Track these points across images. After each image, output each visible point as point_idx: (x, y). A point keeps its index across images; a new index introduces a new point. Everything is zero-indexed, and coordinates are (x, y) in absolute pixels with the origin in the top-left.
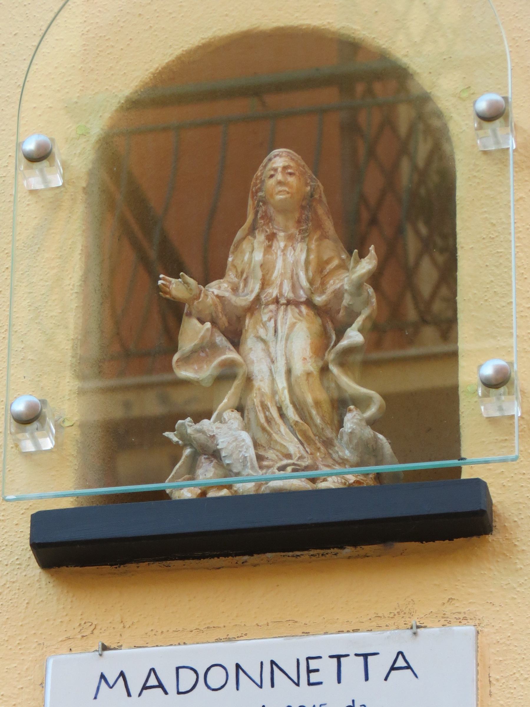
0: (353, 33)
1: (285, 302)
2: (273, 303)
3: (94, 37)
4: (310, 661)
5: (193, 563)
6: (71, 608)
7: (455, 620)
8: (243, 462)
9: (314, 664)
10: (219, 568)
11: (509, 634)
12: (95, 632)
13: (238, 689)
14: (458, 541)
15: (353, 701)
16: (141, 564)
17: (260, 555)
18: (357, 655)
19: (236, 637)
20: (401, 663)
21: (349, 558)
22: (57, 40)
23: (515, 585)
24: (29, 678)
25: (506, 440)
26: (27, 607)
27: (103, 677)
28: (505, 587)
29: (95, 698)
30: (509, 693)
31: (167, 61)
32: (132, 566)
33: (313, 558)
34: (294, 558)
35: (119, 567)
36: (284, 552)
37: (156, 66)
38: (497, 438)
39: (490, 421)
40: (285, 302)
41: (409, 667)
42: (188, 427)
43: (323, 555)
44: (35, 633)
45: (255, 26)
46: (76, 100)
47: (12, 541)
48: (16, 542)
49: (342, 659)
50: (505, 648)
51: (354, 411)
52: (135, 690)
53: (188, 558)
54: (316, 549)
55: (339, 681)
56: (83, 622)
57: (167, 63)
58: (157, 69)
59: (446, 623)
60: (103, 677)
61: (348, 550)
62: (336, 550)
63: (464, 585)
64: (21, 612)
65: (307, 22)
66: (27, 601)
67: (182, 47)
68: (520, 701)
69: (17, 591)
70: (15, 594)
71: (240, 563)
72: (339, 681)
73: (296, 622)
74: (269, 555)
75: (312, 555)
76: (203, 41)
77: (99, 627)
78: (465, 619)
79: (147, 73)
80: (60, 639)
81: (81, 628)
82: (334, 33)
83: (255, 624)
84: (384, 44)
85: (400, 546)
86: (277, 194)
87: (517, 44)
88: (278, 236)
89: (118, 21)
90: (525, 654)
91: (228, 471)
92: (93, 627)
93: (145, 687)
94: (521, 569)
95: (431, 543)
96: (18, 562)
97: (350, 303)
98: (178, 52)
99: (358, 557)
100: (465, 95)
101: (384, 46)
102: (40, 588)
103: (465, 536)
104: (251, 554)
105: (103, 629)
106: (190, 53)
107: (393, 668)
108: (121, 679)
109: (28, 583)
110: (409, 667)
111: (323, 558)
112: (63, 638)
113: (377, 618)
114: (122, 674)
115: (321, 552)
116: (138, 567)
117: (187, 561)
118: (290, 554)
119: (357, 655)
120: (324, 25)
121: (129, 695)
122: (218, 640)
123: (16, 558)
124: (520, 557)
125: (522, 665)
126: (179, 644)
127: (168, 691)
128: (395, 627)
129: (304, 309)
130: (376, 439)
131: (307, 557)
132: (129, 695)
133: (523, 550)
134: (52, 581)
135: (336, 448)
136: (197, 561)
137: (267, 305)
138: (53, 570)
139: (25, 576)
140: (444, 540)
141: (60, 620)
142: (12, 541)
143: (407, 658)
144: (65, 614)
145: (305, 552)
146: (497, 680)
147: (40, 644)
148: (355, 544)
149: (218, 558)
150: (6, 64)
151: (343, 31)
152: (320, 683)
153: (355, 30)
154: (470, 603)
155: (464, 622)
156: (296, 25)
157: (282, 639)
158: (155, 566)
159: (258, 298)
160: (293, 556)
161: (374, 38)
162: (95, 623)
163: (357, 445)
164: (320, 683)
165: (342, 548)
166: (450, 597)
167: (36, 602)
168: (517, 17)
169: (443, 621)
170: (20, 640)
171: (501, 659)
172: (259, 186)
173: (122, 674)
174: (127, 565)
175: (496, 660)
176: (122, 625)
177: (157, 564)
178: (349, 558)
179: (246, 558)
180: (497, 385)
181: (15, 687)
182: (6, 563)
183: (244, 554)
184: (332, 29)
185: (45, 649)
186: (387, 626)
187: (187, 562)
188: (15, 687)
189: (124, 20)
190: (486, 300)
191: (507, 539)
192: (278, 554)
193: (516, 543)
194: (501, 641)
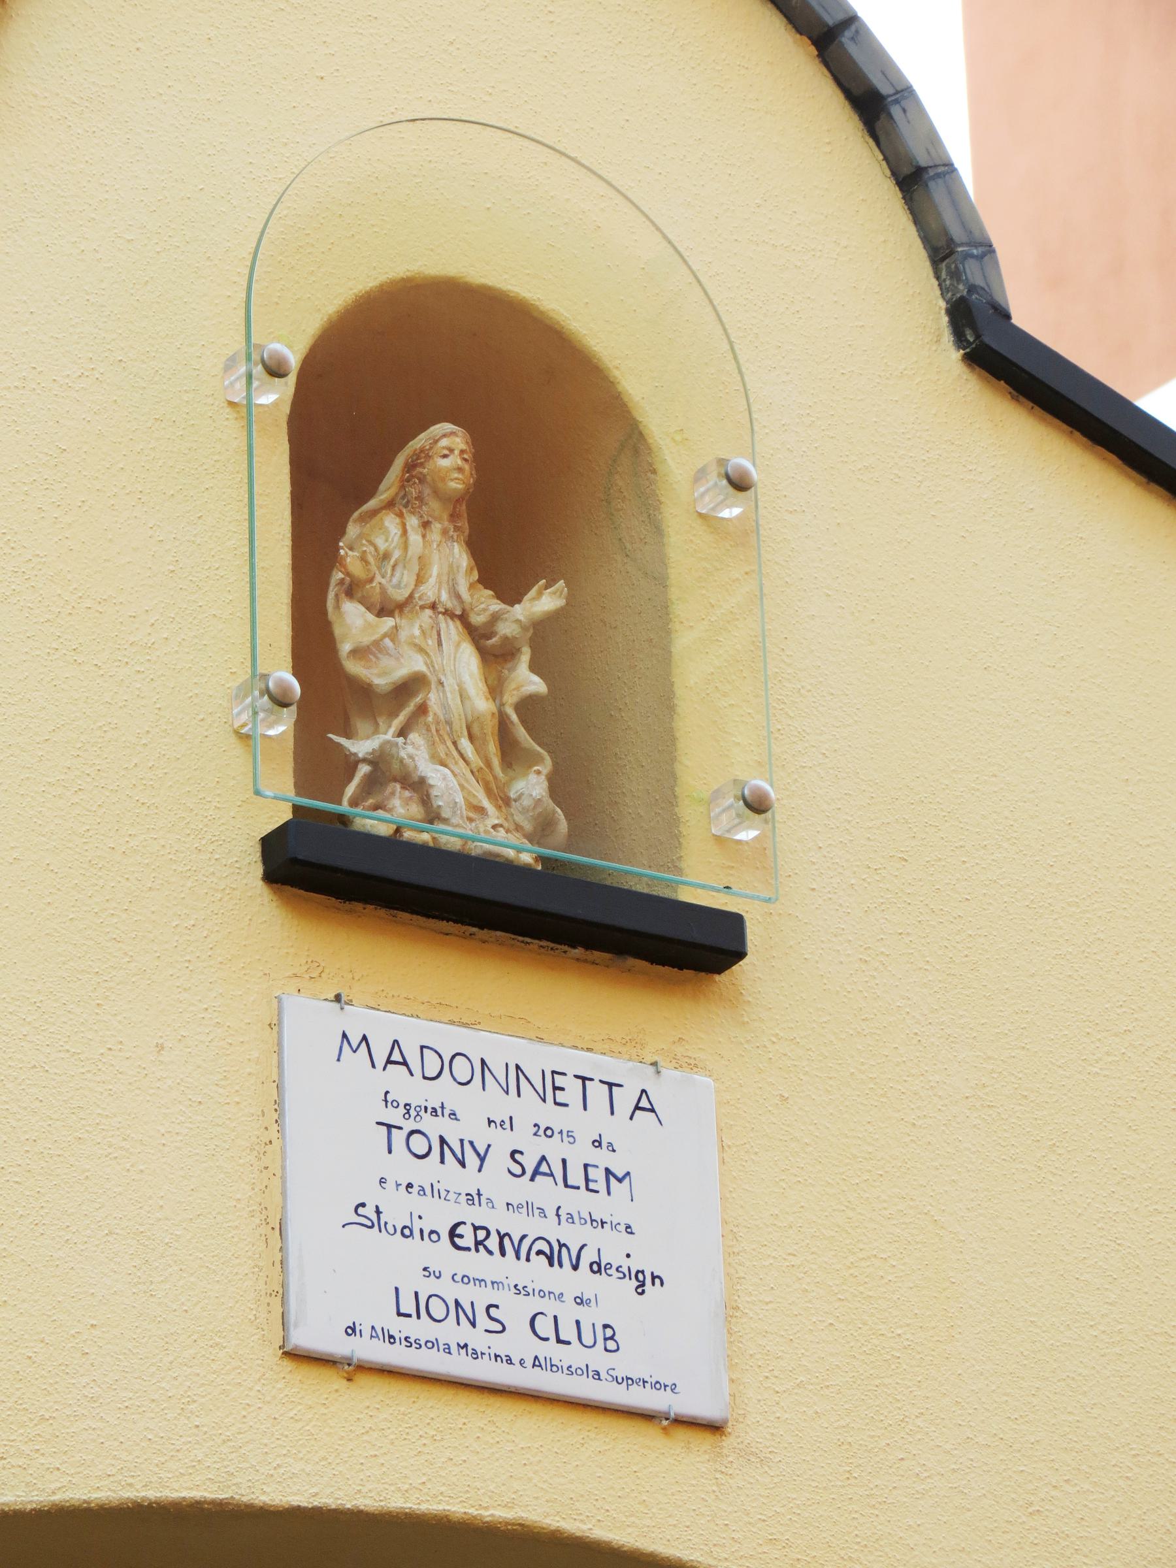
0: (563, 321)
1: (444, 611)
2: (429, 608)
3: (292, 226)
4: (424, 1050)
5: (421, 920)
6: (296, 939)
7: (686, 1065)
8: (453, 808)
9: (559, 1081)
10: (447, 934)
11: (739, 1097)
12: (323, 975)
13: (484, 1089)
14: (688, 973)
15: (600, 1135)
16: (368, 906)
17: (490, 931)
18: (601, 1081)
19: (469, 1023)
20: (644, 1103)
21: (578, 960)
22: (249, 217)
23: (743, 1041)
24: (256, 1013)
25: (733, 867)
26: (249, 924)
27: (344, 1036)
28: (733, 1039)
29: (338, 1060)
30: (741, 1165)
31: (371, 285)
32: (359, 906)
33: (542, 950)
34: (523, 944)
35: (345, 902)
36: (515, 934)
37: (361, 287)
38: (724, 862)
39: (716, 839)
40: (444, 611)
41: (652, 1110)
42: (401, 749)
43: (552, 949)
44: (259, 960)
45: (462, 275)
46: (276, 300)
47: (230, 837)
48: (233, 839)
49: (614, 1088)
50: (735, 1111)
51: (393, 737)
52: (379, 1063)
53: (418, 913)
54: (548, 941)
55: (585, 1109)
56: (310, 960)
57: (371, 288)
58: (361, 291)
59: (677, 1066)
60: (344, 1036)
61: (578, 952)
62: (566, 948)
63: (693, 1026)
64: (243, 929)
65: (516, 289)
66: (249, 917)
67: (386, 273)
68: (751, 1177)
69: (238, 902)
70: (236, 904)
71: (467, 934)
72: (585, 1109)
73: (529, 1022)
74: (499, 933)
75: (541, 946)
76: (409, 274)
77: (327, 971)
78: (696, 1066)
79: (351, 292)
80: (287, 975)
81: (308, 966)
82: (542, 312)
83: (487, 1013)
84: (595, 346)
85: (632, 962)
86: (452, 480)
87: (727, 391)
88: (432, 526)
89: (318, 215)
90: (754, 1124)
91: (433, 816)
92: (320, 969)
93: (389, 1061)
94: (748, 1022)
95: (660, 967)
96: (237, 865)
97: (517, 636)
98: (383, 278)
99: (586, 961)
100: (678, 438)
101: (595, 349)
102: (262, 904)
103: (695, 970)
104: (482, 928)
105: (332, 974)
106: (393, 283)
107: (637, 1108)
108: (364, 1043)
109: (249, 894)
110: (652, 1110)
111: (552, 952)
112: (289, 973)
113: (609, 1041)
114: (364, 1038)
115: (552, 945)
116: (364, 909)
117: (415, 916)
118: (521, 938)
119: (601, 1081)
120: (534, 300)
121: (373, 1066)
122: (452, 1023)
123: (235, 859)
124: (746, 1009)
125: (752, 1135)
126: (412, 1016)
127: (414, 1073)
128: (628, 1057)
129: (458, 623)
130: (554, 812)
131: (536, 946)
132: (373, 1066)
133: (749, 1002)
134: (275, 899)
135: (512, 810)
136: (424, 919)
137: (422, 608)
138: (275, 886)
139: (246, 885)
140: (673, 968)
141: (285, 951)
142: (230, 837)
143: (526, 1073)
144: (291, 944)
145: (537, 941)
146: (729, 1147)
147: (265, 974)
148: (589, 946)
149: (448, 922)
150: (193, 224)
151: (552, 314)
152: (566, 1105)
153: (566, 317)
154: (700, 1049)
155: (695, 1070)
156: (505, 288)
157: (526, 1041)
158: (382, 912)
159: (411, 596)
160: (523, 942)
161: (585, 335)
162: (323, 964)
163: (540, 814)
164: (566, 1105)
165: (574, 947)
166: (680, 1036)
167: (260, 921)
168: (725, 357)
169: (674, 1064)
170: (244, 963)
171: (732, 1123)
172: (422, 460)
173: (364, 1038)
174: (353, 902)
175: (727, 1123)
176: (350, 976)
177: (383, 910)
178: (578, 960)
179: (474, 930)
180: (757, 810)
181: (242, 1020)
182: (224, 863)
183: (474, 926)
184: (542, 308)
185: (271, 982)
186: (620, 1053)
187: (415, 917)
188: (242, 1020)
189: (324, 216)
190: (708, 694)
191: (733, 984)
192: (507, 935)
193: (743, 991)
194: (731, 1103)
